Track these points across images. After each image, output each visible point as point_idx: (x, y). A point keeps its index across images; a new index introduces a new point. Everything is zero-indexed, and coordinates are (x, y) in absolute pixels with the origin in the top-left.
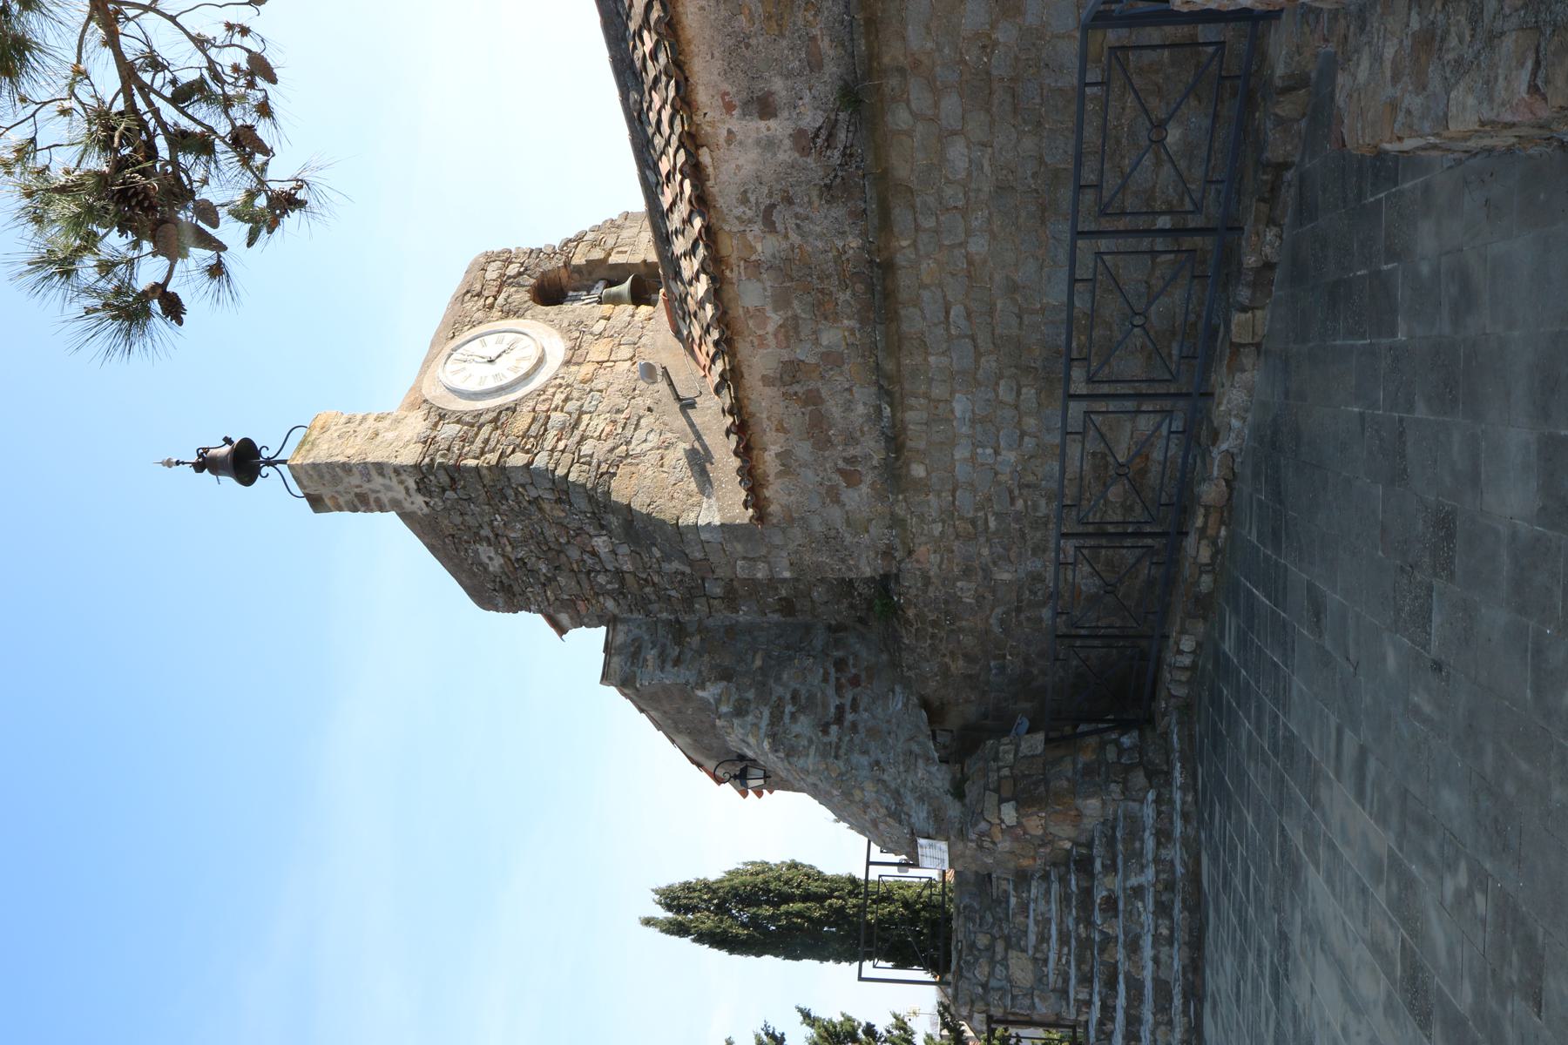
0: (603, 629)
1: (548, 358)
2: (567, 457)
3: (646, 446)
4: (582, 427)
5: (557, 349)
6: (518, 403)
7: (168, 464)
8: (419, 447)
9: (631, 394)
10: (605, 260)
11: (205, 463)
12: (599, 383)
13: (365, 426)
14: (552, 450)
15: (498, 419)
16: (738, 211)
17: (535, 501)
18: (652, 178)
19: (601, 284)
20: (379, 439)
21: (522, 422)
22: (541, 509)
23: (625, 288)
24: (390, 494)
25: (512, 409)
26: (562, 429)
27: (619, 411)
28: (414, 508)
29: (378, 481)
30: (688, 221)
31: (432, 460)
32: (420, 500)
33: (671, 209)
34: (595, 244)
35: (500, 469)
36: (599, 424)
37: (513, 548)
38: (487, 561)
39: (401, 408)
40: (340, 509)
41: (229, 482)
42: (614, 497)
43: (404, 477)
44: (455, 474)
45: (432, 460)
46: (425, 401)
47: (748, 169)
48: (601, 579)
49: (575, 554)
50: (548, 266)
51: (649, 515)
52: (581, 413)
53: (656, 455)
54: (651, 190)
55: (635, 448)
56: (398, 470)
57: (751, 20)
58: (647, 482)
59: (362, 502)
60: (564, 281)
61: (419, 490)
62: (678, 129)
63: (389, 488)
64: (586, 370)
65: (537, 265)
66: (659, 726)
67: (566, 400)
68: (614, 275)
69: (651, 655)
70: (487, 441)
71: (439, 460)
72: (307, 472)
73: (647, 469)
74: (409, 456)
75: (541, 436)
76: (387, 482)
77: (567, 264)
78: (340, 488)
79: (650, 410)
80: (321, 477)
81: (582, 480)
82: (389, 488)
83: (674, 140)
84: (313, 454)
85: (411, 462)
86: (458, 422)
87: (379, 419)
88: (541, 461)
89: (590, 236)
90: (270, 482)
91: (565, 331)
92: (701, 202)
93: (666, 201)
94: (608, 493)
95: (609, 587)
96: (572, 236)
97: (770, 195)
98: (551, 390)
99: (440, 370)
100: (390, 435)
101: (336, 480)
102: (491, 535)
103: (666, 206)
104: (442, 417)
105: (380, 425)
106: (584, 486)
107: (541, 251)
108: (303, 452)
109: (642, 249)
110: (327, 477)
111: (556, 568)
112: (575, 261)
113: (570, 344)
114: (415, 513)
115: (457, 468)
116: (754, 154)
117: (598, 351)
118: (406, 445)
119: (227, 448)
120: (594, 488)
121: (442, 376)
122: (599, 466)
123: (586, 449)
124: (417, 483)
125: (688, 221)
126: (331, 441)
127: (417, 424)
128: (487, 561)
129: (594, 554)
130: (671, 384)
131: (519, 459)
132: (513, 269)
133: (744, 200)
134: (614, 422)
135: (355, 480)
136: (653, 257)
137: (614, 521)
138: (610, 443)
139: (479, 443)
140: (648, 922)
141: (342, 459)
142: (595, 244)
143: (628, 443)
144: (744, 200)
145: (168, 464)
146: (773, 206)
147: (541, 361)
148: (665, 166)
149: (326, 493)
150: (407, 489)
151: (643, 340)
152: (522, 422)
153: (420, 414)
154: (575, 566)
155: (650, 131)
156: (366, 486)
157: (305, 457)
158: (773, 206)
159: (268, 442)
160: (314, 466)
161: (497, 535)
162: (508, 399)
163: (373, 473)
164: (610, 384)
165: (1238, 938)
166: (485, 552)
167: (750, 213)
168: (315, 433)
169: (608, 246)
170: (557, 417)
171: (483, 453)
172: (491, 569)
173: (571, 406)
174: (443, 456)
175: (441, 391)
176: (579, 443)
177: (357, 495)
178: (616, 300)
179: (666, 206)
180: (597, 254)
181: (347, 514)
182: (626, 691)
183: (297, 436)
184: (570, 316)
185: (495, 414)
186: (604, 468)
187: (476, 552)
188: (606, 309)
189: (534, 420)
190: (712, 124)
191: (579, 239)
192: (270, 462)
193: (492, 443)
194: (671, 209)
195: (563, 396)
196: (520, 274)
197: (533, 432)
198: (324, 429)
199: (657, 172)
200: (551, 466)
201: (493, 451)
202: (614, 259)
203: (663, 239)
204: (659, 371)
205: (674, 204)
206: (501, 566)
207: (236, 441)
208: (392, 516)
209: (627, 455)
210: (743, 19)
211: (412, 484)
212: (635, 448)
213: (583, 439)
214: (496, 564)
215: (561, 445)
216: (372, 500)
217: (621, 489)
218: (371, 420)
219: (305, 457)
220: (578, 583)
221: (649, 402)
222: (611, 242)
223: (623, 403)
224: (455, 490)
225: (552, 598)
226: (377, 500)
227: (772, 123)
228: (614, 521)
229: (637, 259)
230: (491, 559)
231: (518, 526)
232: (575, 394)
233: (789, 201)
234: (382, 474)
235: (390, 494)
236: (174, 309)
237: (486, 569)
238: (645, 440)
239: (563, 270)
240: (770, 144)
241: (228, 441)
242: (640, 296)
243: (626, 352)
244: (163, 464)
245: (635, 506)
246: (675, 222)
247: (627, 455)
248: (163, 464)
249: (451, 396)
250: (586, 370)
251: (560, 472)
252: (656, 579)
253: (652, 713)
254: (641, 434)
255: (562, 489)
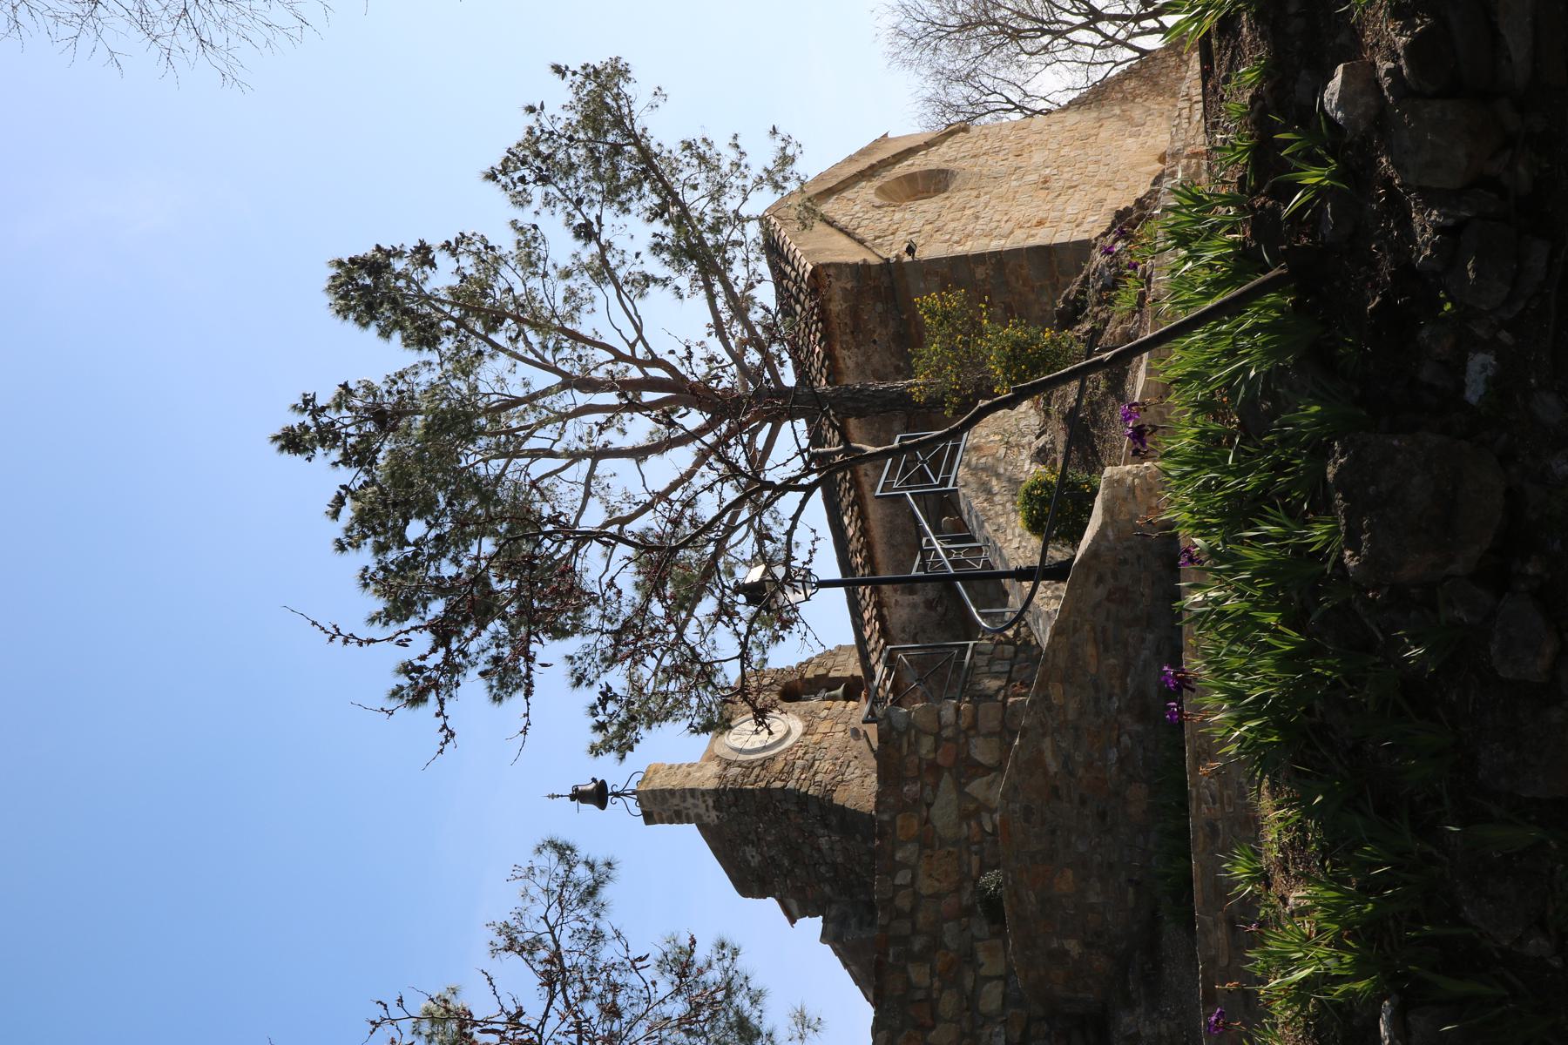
0: (821, 918)
1: (793, 731)
2: (807, 783)
3: (855, 776)
4: (815, 768)
5: (798, 726)
6: (775, 756)
7: (553, 796)
8: (717, 780)
9: (845, 749)
10: (825, 676)
12: (825, 744)
13: (681, 770)
14: (798, 780)
15: (764, 764)
16: (902, 635)
17: (786, 812)
18: (859, 622)
19: (823, 691)
20: (691, 777)
21: (779, 766)
22: (789, 819)
23: (840, 691)
24: (696, 811)
25: (772, 759)
26: (803, 769)
27: (837, 759)
28: (709, 820)
29: (690, 801)
30: (878, 642)
32: (714, 814)
33: (869, 638)
34: (819, 665)
35: (767, 790)
36: (826, 765)
37: (769, 848)
38: (750, 858)
39: (702, 760)
40: (662, 822)
42: (835, 802)
43: (706, 798)
44: (739, 793)
46: (718, 756)
47: (905, 617)
48: (823, 869)
49: (807, 850)
50: (789, 679)
51: (855, 810)
52: (814, 760)
53: (859, 780)
54: (858, 627)
55: (847, 777)
56: (704, 793)
57: (904, 555)
58: (854, 794)
59: (678, 817)
60: (799, 688)
61: (714, 807)
62: (873, 600)
63: (696, 806)
64: (816, 737)
65: (782, 678)
66: (857, 982)
67: (805, 754)
68: (832, 683)
69: (853, 921)
70: (758, 776)
71: (729, 786)
72: (647, 796)
73: (855, 788)
74: (712, 784)
75: (790, 773)
76: (696, 802)
77: (802, 677)
78: (665, 807)
79: (856, 757)
80: (655, 799)
81: (816, 794)
82: (696, 806)
83: (871, 604)
85: (713, 788)
87: (690, 766)
88: (791, 785)
89: (816, 661)
90: (615, 807)
91: (802, 717)
92: (884, 632)
93: (867, 634)
94: (832, 800)
95: (827, 875)
96: (804, 661)
97: (915, 628)
100: (698, 774)
101: (664, 801)
102: (755, 839)
103: (867, 637)
104: (729, 764)
106: (817, 797)
107: (784, 669)
108: (645, 783)
109: (853, 668)
110: (659, 798)
111: (795, 862)
112: (807, 676)
113: (806, 724)
114: (709, 824)
115: (741, 790)
116: (907, 610)
117: (823, 727)
118: (708, 779)
119: (594, 784)
120: (823, 798)
121: (727, 742)
122: (826, 787)
123: (818, 778)
124: (714, 802)
125: (878, 642)
126: (661, 778)
127: (713, 768)
128: (750, 858)
129: (819, 850)
130: (868, 741)
131: (778, 784)
132: (766, 681)
133: (903, 631)
134: (834, 764)
135: (676, 801)
136: (859, 672)
137: (834, 820)
138: (832, 775)
139: (753, 777)
141: (670, 787)
142: (819, 665)
143: (843, 775)
144: (903, 631)
145: (553, 796)
146: (916, 634)
147: (788, 733)
148: (866, 615)
149: (656, 809)
150: (707, 806)
151: (852, 720)
153: (715, 763)
154: (807, 861)
155: (859, 597)
156: (682, 805)
158: (916, 634)
160: (653, 791)
161: (759, 839)
162: (772, 753)
163: (688, 795)
164: (831, 745)
166: (750, 851)
167: (906, 637)
168: (650, 775)
169: (828, 667)
170: (800, 763)
171: (756, 782)
172: (752, 864)
173: (807, 757)
175: (727, 750)
176: (814, 775)
177: (675, 811)
178: (834, 698)
179: (867, 637)
180: (821, 671)
181: (667, 825)
182: (837, 947)
183: (639, 777)
184: (805, 708)
186: (829, 787)
187: (744, 852)
188: (828, 703)
189: (786, 764)
190: (888, 597)
191: (809, 662)
193: (761, 777)
194: (869, 638)
196: (771, 684)
198: (656, 772)
199: (862, 618)
200: (798, 787)
201: (762, 781)
202: (832, 674)
203: (864, 657)
204: (862, 733)
205: (871, 634)
206: (759, 862)
207: (599, 780)
208: (692, 828)
209: (843, 781)
210: (901, 555)
211: (710, 803)
212: (847, 777)
213: (816, 773)
214: (755, 861)
215: (803, 777)
216: (684, 815)
217: (839, 798)
218: (684, 767)
220: (808, 873)
221: (855, 754)
222: (830, 664)
223: (840, 754)
224: (736, 806)
225: (790, 886)
226: (687, 815)
227: (915, 597)
228: (834, 820)
229: (848, 674)
230: (753, 857)
231: (773, 832)
232: (810, 750)
233: (924, 631)
234: (693, 796)
235: (696, 811)
236: (784, 639)
237: (749, 865)
238: (853, 773)
239: (799, 682)
240: (914, 606)
241: (594, 780)
242: (850, 695)
243: (841, 727)
244: (549, 796)
245: (847, 805)
246: (872, 644)
247: (843, 781)
248: (549, 796)
249: (734, 753)
250: (816, 737)
251: (803, 790)
252: (857, 869)
253: (853, 968)
254: (850, 770)
255: (802, 799)
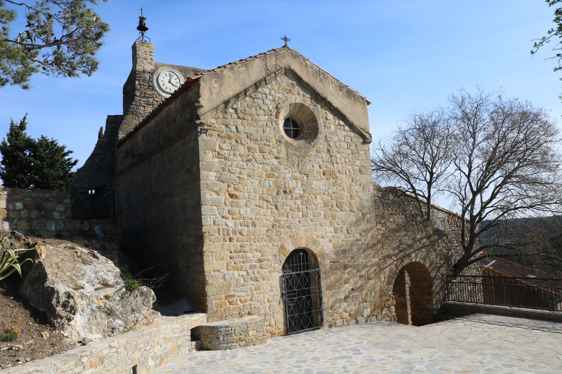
6: (156, 90)
11: (142, 19)
20: (145, 60)
25: (154, 89)
31: (138, 74)
41: (138, 24)
45: (138, 74)
84: (140, 46)
86: (150, 78)
98: (160, 97)
99: (167, 70)
105: (149, 59)
140: (560, 37)
152: (149, 92)
157: (138, 44)
159: (147, 33)
165: (488, 347)
174: (139, 76)
185: (152, 85)
189: (151, 95)
192: (143, 34)
195: (158, 100)
197: (146, 95)
198: (148, 47)
219: (138, 44)
249: (158, 74)
